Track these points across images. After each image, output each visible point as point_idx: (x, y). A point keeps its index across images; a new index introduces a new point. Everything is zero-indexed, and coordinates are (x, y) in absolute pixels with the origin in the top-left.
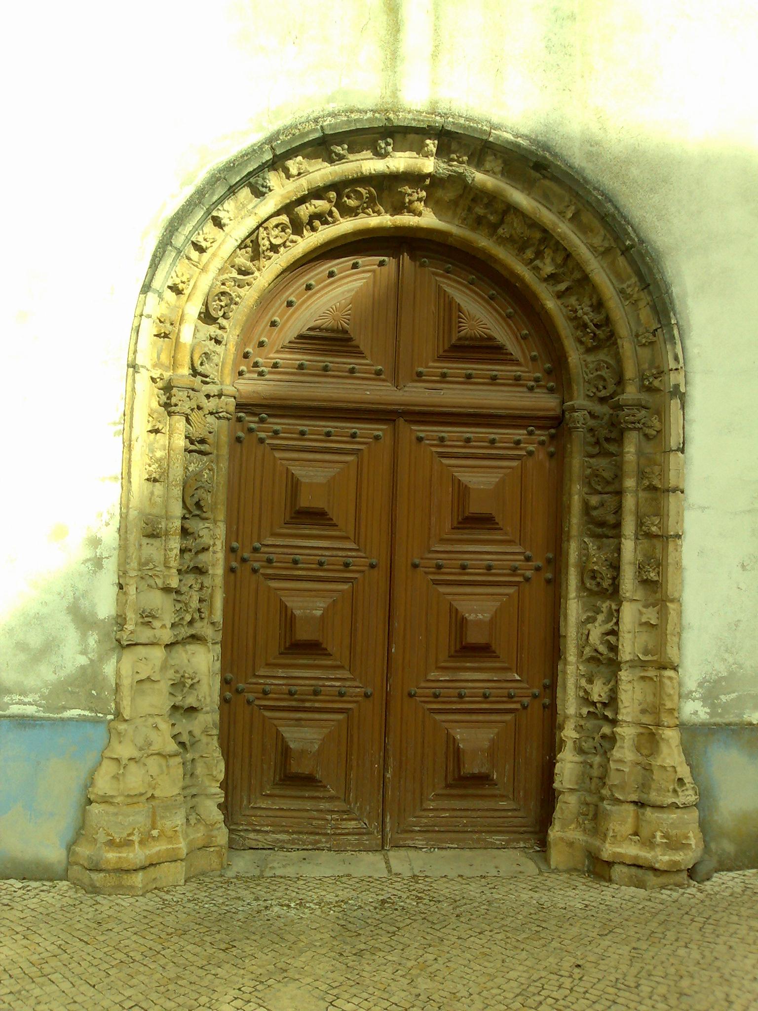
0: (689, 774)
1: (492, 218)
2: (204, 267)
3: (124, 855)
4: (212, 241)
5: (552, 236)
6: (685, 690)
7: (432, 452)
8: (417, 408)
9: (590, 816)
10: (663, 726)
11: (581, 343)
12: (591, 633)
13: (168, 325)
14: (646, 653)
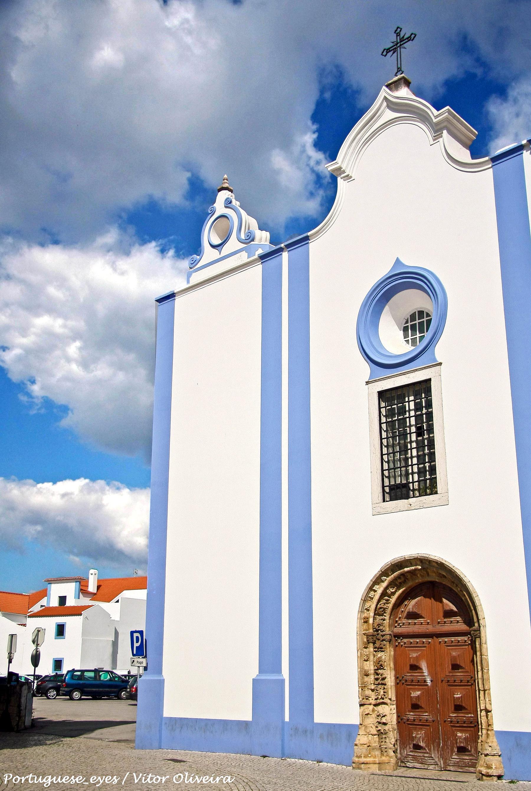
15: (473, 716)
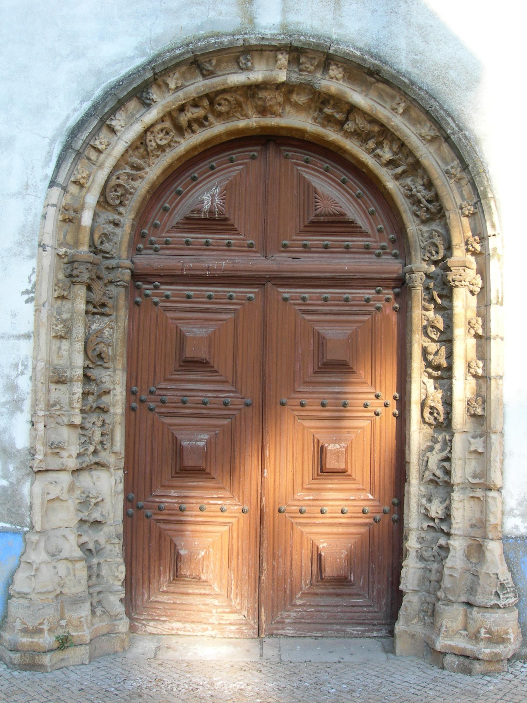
0: (510, 580)
1: (338, 116)
2: (101, 165)
3: (35, 640)
4: (106, 144)
5: (389, 130)
6: (507, 508)
7: (296, 310)
8: (285, 274)
9: (429, 614)
10: (488, 538)
11: (417, 216)
12: (430, 460)
13: (71, 212)
14: (474, 476)
15: (371, 497)
